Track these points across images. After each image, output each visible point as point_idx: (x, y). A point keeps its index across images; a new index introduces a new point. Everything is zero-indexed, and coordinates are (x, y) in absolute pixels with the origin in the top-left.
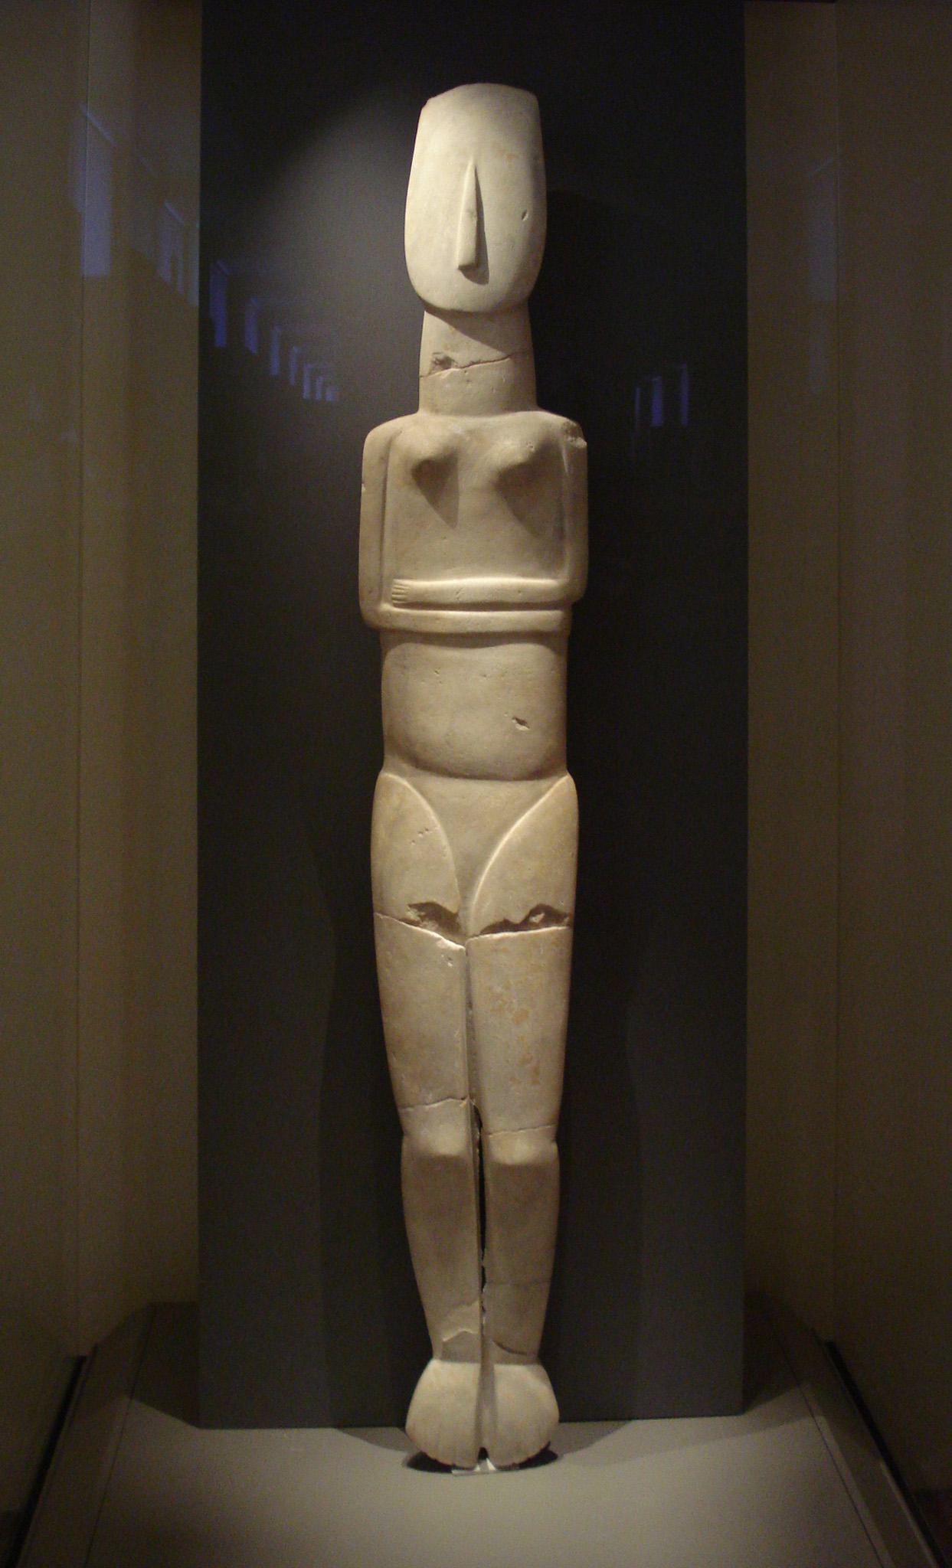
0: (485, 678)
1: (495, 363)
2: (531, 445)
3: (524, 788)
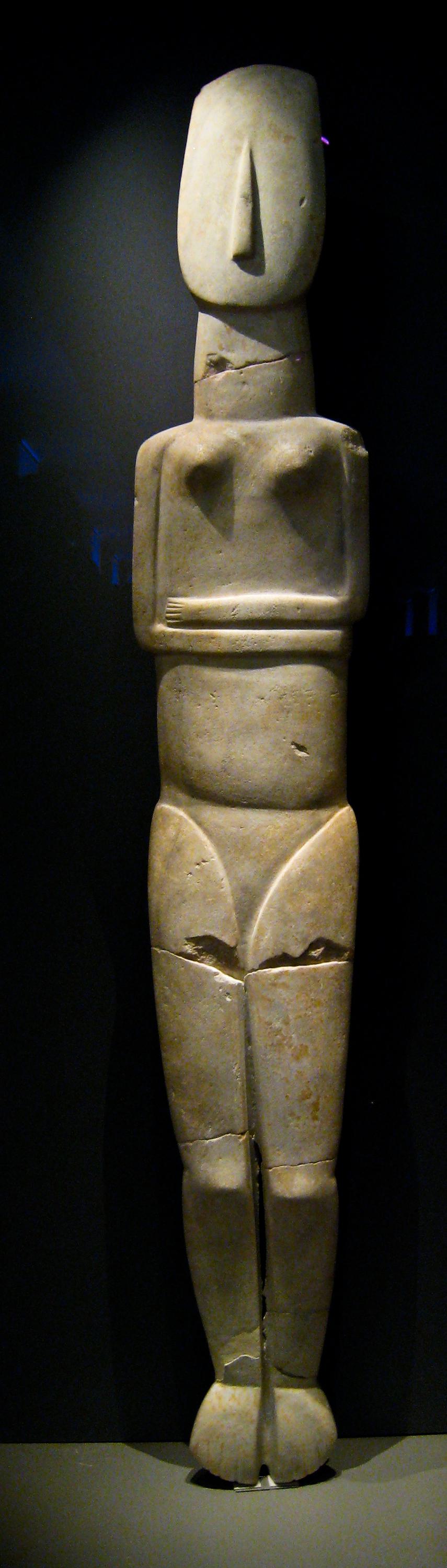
1: (273, 363)
3: (302, 818)
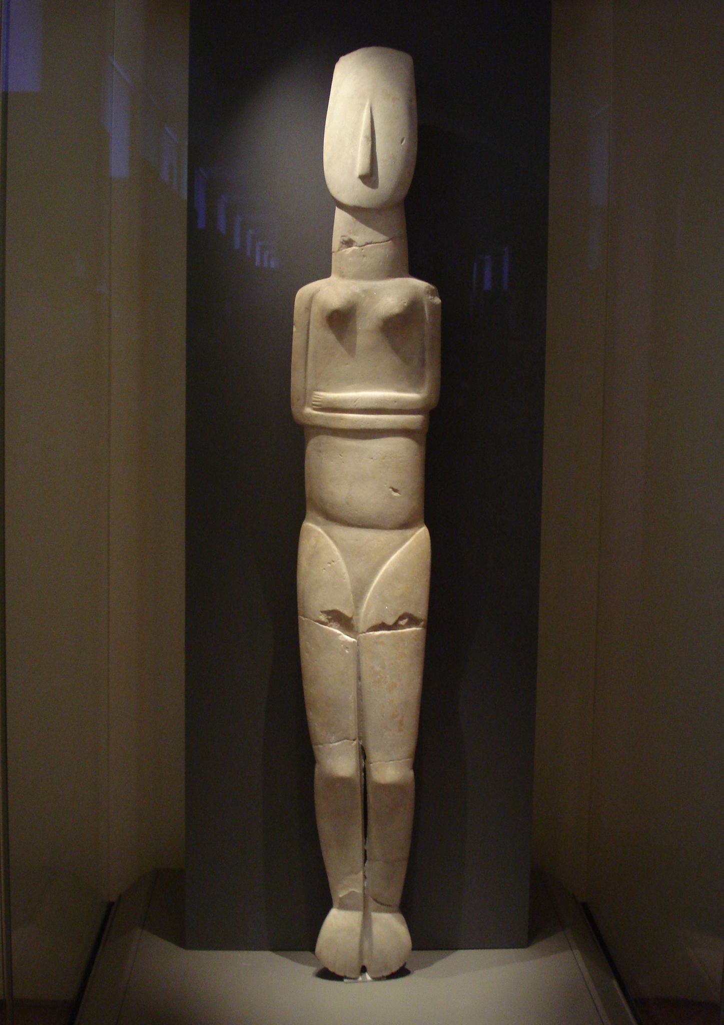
1: (382, 244)
3: (396, 535)
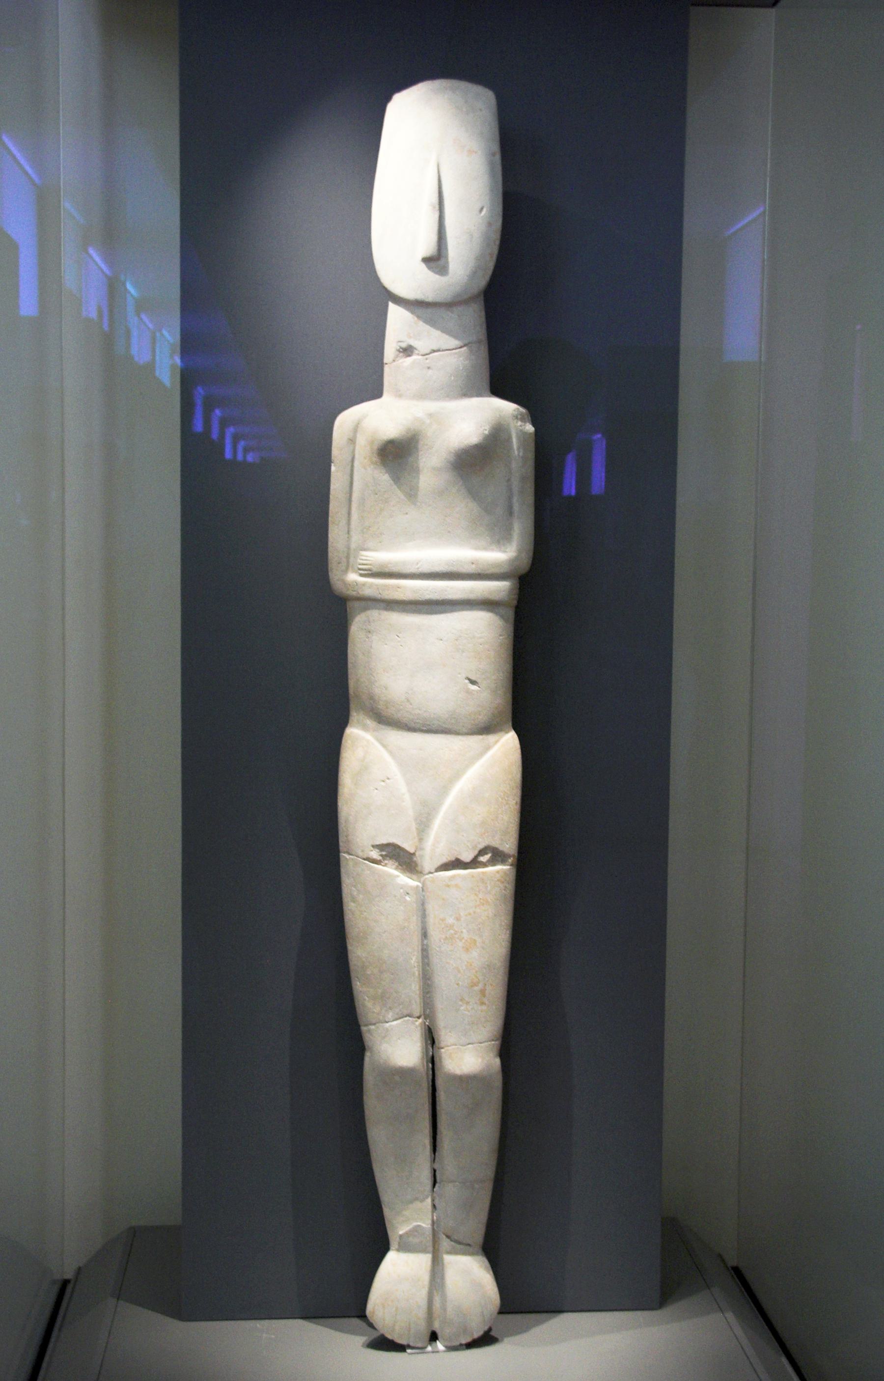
0: (441, 642)
1: (454, 351)
2: (486, 428)
3: (475, 741)
